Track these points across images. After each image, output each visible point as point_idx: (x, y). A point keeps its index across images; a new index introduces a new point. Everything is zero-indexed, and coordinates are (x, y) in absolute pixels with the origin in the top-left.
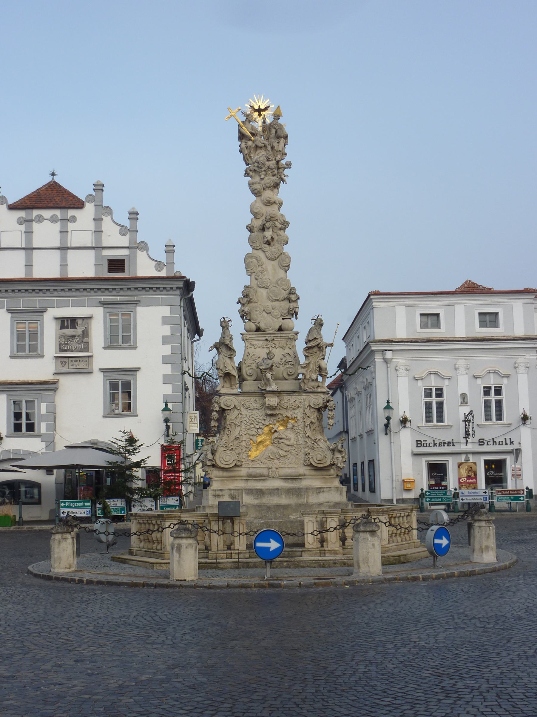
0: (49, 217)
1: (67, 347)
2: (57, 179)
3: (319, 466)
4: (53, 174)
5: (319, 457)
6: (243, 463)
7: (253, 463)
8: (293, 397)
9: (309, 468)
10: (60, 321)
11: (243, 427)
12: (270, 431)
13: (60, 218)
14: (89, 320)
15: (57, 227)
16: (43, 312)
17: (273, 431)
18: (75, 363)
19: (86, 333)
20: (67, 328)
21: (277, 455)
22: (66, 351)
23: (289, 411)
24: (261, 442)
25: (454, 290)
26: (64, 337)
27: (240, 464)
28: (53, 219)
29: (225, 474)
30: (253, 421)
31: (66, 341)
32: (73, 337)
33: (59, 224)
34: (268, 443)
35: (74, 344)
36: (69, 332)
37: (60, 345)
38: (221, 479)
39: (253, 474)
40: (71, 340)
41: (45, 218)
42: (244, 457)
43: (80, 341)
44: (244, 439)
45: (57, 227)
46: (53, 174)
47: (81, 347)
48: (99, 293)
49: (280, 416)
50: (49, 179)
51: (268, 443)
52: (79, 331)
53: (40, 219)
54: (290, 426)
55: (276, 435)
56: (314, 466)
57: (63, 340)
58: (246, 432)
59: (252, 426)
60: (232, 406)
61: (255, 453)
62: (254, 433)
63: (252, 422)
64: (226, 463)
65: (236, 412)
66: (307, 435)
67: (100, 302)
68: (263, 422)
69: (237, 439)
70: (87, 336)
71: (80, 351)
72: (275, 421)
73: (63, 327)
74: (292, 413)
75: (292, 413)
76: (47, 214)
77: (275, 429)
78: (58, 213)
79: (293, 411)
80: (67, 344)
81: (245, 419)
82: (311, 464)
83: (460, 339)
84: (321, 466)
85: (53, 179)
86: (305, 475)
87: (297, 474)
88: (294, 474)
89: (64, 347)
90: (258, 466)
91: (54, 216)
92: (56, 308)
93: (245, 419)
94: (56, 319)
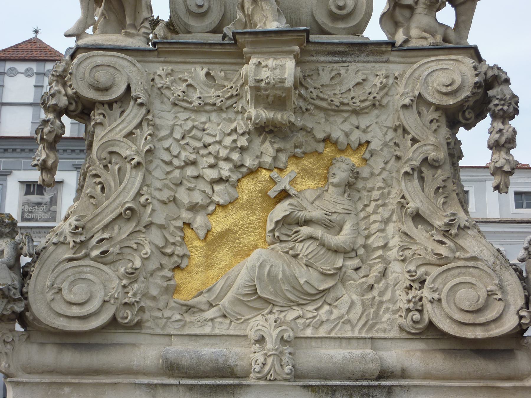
0: (23, 71)
1: (30, 216)
2: (39, 36)
3: (469, 333)
4: (37, 32)
5: (467, 297)
6: (146, 316)
7: (188, 318)
8: (353, 67)
9: (419, 345)
10: (25, 187)
11: (158, 173)
12: (264, 193)
13: (35, 71)
14: (58, 186)
15: (33, 81)
16: (6, 175)
17: (273, 193)
18: (39, 235)
19: (53, 201)
20: (33, 193)
21: (285, 287)
22: (29, 220)
23: (339, 119)
24: (224, 234)
25: (485, 165)
26: (28, 204)
27: (129, 315)
28: (28, 73)
29: (69, 358)
30: (196, 150)
31: (30, 209)
32: (39, 204)
33: (35, 77)
34: (250, 239)
35: (39, 213)
36: (35, 198)
37: (23, 213)
38: (47, 379)
39: (185, 361)
40: (36, 207)
41: (20, 71)
42: (154, 292)
43: (47, 210)
44: (159, 219)
45: (33, 81)
46: (37, 32)
47: (47, 216)
48: (73, 155)
49: (300, 137)
50: (32, 35)
51: (250, 239)
52: (47, 197)
53: (13, 73)
54: (340, 174)
55: (281, 210)
56: (443, 335)
57: (27, 208)
58: (165, 195)
59: (190, 171)
60: (118, 91)
61: (200, 276)
62: (198, 198)
63: (193, 157)
64: (76, 311)
65: (133, 115)
66: (412, 206)
67: (73, 165)
68: (235, 156)
69: (130, 214)
70: (56, 204)
71: (46, 221)
72: (283, 157)
73: (28, 193)
74: (347, 127)
75: (347, 127)
76: (21, 67)
77: (284, 184)
78: (34, 66)
79: (354, 120)
80: (31, 212)
81: (166, 144)
82: (431, 324)
83: (494, 220)
84: (479, 333)
85: (36, 36)
86: (404, 374)
87: (373, 367)
88: (358, 367)
89: (28, 215)
90: (207, 330)
91: (28, 70)
92: (22, 172)
93: (166, 144)
94: (21, 182)
